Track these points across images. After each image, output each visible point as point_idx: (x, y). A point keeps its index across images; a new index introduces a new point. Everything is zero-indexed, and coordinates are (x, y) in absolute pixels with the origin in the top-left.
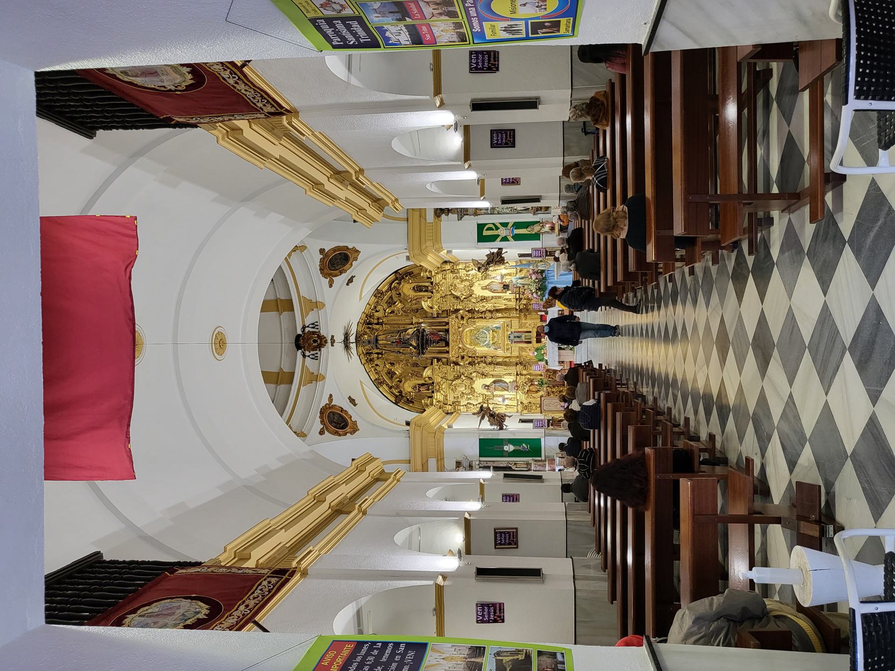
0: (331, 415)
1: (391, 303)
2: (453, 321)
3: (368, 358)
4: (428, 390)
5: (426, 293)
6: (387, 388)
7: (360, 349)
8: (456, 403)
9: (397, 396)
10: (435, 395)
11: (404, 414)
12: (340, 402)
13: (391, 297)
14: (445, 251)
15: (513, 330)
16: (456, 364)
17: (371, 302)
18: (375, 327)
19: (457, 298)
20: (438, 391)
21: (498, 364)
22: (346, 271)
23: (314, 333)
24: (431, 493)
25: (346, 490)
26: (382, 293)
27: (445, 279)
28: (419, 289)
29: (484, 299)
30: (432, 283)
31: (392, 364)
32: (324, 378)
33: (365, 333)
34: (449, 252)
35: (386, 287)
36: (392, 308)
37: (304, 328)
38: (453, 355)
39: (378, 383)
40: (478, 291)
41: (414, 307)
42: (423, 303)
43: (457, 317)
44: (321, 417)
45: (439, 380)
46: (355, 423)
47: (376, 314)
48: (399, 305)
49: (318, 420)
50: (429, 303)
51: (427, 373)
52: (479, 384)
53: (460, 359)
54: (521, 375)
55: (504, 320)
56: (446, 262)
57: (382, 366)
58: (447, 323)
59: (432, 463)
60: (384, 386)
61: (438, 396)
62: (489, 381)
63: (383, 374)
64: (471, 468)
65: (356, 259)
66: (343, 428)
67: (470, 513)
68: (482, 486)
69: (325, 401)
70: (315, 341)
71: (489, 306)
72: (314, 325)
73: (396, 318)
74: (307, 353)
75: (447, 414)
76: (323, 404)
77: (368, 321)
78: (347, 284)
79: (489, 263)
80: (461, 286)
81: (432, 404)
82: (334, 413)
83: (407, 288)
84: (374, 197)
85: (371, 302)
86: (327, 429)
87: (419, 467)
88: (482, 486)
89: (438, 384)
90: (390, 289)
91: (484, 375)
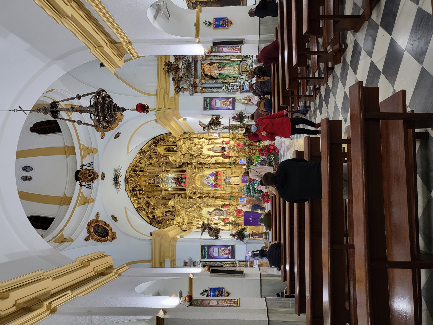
0: (97, 227)
1: (150, 158)
2: (189, 169)
3: (134, 193)
4: (172, 215)
5: (173, 152)
6: (145, 214)
7: (127, 187)
8: (190, 224)
9: (151, 219)
10: (176, 218)
11: (152, 229)
12: (105, 218)
13: (150, 155)
14: (182, 119)
15: (227, 176)
16: (191, 198)
17: (137, 158)
18: (138, 173)
19: (192, 155)
20: (178, 215)
21: (217, 198)
22: (113, 128)
23: (89, 170)
24: (143, 286)
25: (50, 285)
26: (144, 152)
27: (185, 143)
28: (168, 150)
29: (209, 156)
30: (176, 146)
31: (149, 198)
32: (93, 201)
33: (132, 177)
34: (185, 119)
35: (147, 149)
36: (151, 161)
37: (82, 166)
38: (188, 192)
39: (139, 210)
40: (206, 152)
41: (165, 161)
42: (170, 157)
43: (192, 167)
44: (88, 228)
45: (179, 208)
46: (114, 234)
47: (140, 165)
48: (156, 160)
49: (85, 230)
50: (174, 158)
51: (171, 203)
52: (205, 211)
53: (193, 194)
54: (232, 205)
55: (222, 169)
56: (185, 133)
57: (142, 199)
58: (185, 171)
59: (168, 262)
60: (143, 212)
61: (178, 219)
62: (211, 209)
63: (143, 204)
64: (194, 265)
65: (121, 120)
66: (105, 236)
67: (165, 311)
68: (191, 280)
69: (93, 217)
70: (90, 176)
71: (213, 161)
72: (90, 165)
73: (153, 168)
74: (83, 184)
75: (184, 231)
76: (91, 219)
77: (134, 170)
78: (115, 138)
79: (210, 124)
80: (195, 148)
81: (173, 224)
82: (99, 226)
83: (161, 150)
84: (112, 39)
85: (137, 158)
86: (92, 236)
87: (158, 264)
88: (191, 280)
89: (179, 211)
90: (150, 149)
91: (208, 205)
